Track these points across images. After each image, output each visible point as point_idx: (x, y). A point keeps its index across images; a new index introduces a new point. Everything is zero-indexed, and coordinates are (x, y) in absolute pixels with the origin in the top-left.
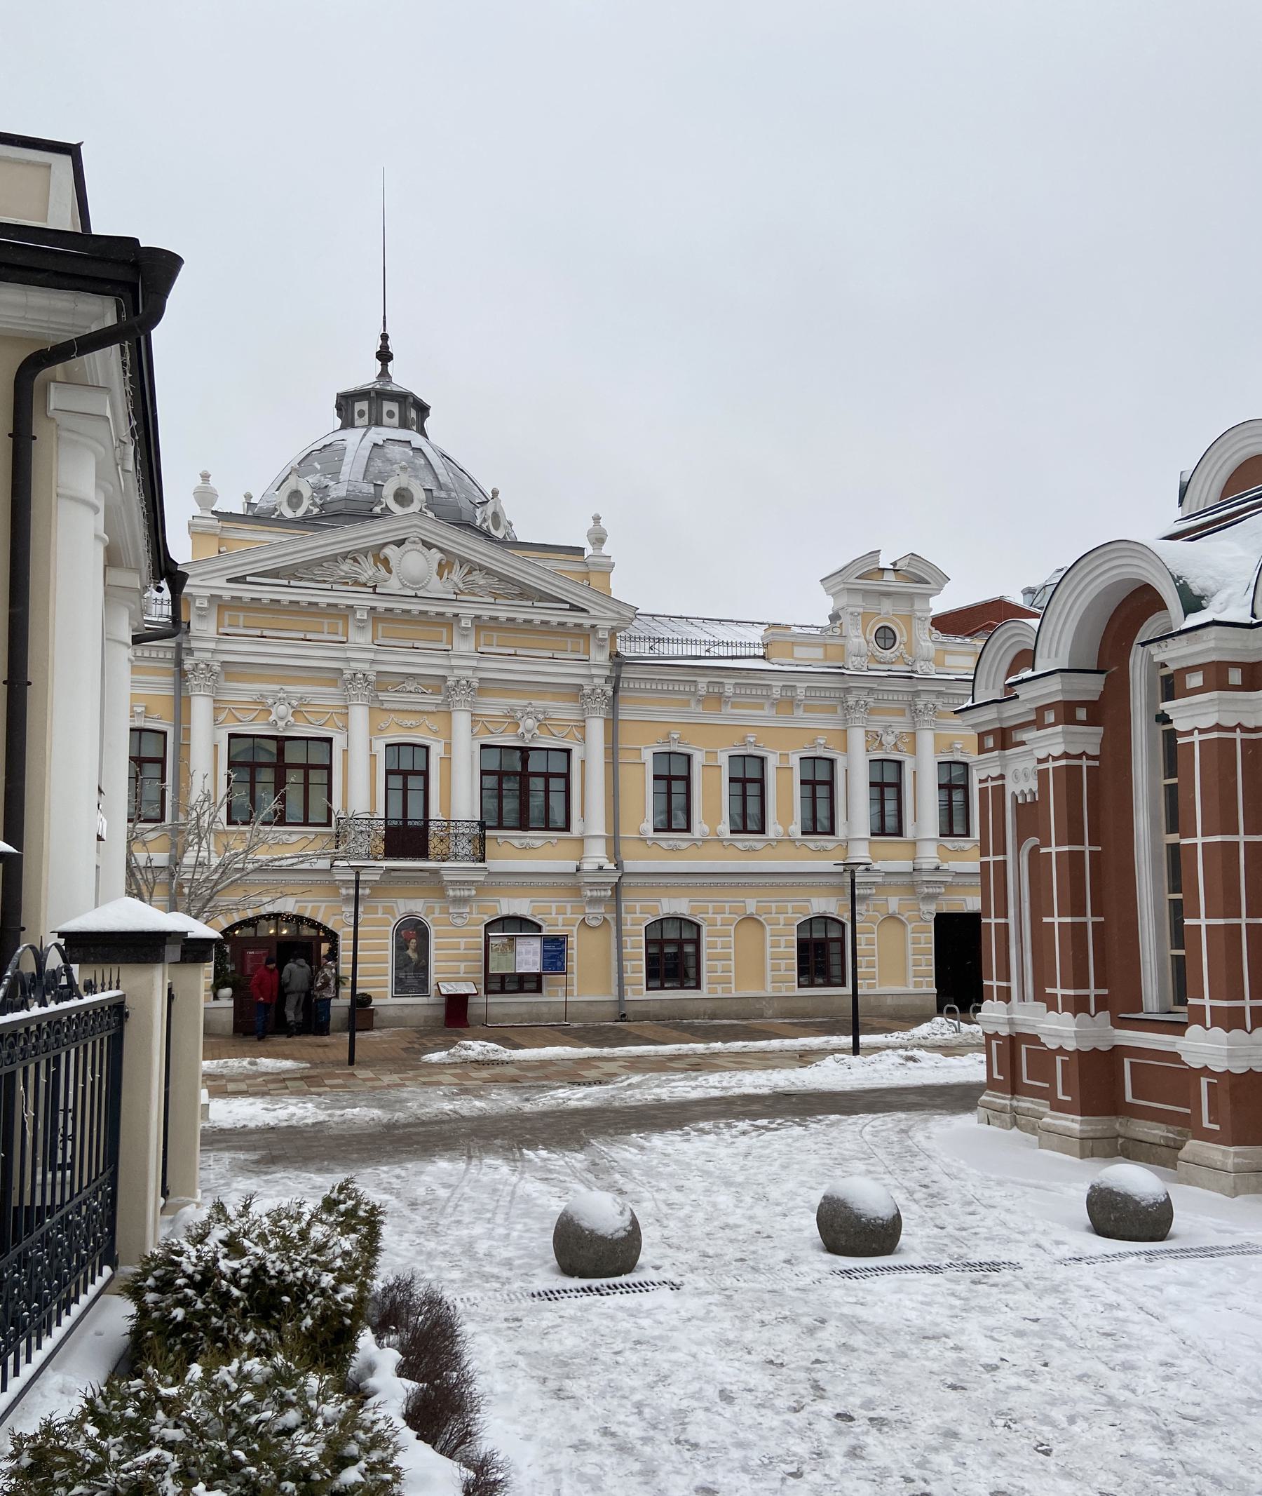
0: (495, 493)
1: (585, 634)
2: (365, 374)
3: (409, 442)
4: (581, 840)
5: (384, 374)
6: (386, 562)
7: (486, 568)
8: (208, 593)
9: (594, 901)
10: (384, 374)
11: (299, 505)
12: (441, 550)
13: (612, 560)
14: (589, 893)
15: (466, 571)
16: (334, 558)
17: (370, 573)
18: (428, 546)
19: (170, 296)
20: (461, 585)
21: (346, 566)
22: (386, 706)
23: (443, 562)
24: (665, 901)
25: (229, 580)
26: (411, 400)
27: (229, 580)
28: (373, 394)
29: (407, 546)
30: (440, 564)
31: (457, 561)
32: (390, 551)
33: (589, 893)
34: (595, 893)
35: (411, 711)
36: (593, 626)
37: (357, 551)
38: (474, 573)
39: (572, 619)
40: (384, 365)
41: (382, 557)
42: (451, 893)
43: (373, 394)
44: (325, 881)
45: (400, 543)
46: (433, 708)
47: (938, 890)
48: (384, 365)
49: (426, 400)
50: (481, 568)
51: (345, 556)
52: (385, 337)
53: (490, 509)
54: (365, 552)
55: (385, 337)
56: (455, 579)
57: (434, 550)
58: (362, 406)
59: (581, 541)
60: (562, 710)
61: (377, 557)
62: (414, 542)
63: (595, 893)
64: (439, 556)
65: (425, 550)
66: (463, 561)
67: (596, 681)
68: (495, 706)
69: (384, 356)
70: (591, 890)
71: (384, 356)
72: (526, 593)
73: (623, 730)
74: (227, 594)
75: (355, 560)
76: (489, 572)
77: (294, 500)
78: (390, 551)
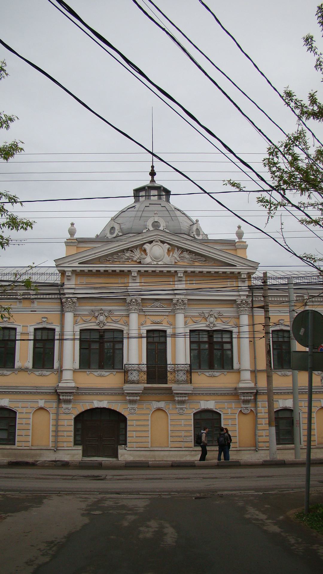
0: (197, 221)
1: (236, 276)
2: (146, 181)
3: (161, 204)
4: (239, 371)
5: (153, 181)
6: (145, 251)
7: (189, 250)
8: (71, 269)
9: (246, 402)
10: (153, 181)
11: (114, 233)
12: (169, 244)
13: (247, 243)
14: (242, 398)
15: (180, 252)
16: (123, 251)
17: (138, 256)
18: (163, 242)
19: (166, 187)
20: (178, 259)
21: (128, 254)
22: (147, 313)
23: (170, 249)
24: (202, 402)
25: (79, 263)
26: (162, 188)
27: (79, 263)
28: (146, 188)
29: (154, 243)
30: (168, 250)
31: (176, 248)
32: (147, 247)
33: (242, 398)
34: (245, 398)
35: (156, 315)
36: (239, 273)
37: (132, 247)
38: (184, 253)
39: (228, 270)
40: (153, 178)
41: (143, 249)
42: (177, 399)
43: (146, 188)
44: (121, 393)
45: (151, 242)
46: (167, 314)
47: (184, 398)
48: (153, 178)
49: (169, 188)
50: (187, 250)
51: (127, 249)
52: (153, 167)
53: (194, 228)
54: (136, 247)
55: (153, 167)
56: (175, 256)
57: (166, 244)
58: (143, 193)
59: (234, 237)
60: (228, 311)
61: (141, 249)
62: (157, 241)
63: (245, 398)
64: (168, 246)
65: (161, 244)
66: (179, 248)
67: (242, 298)
68: (194, 311)
69: (153, 174)
70: (244, 396)
71: (153, 174)
72: (206, 259)
73: (255, 317)
74: (78, 269)
75: (132, 251)
76: (191, 252)
77: (112, 231)
78: (147, 247)
